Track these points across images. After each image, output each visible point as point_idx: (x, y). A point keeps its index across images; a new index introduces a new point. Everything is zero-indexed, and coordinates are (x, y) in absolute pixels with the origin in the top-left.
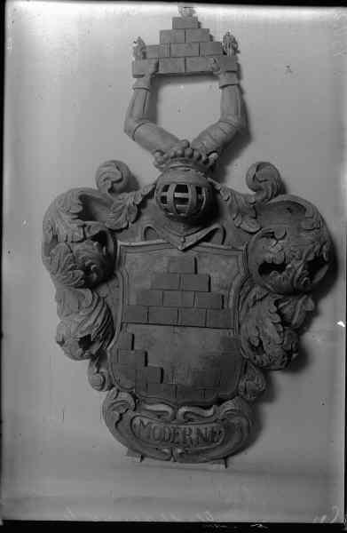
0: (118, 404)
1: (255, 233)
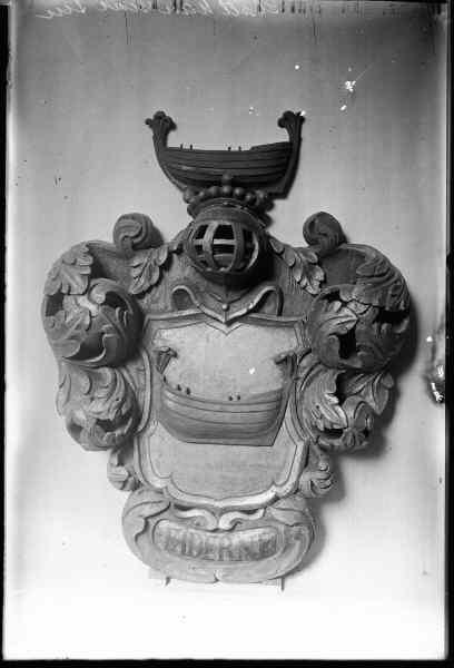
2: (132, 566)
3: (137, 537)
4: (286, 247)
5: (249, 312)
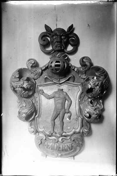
0: (29, 64)
1: (85, 78)
2: (38, 152)
3: (39, 145)
4: (75, 67)
5: (66, 81)
